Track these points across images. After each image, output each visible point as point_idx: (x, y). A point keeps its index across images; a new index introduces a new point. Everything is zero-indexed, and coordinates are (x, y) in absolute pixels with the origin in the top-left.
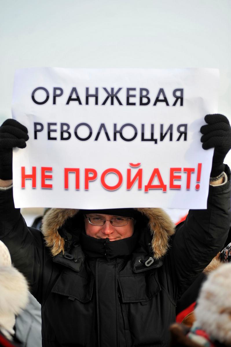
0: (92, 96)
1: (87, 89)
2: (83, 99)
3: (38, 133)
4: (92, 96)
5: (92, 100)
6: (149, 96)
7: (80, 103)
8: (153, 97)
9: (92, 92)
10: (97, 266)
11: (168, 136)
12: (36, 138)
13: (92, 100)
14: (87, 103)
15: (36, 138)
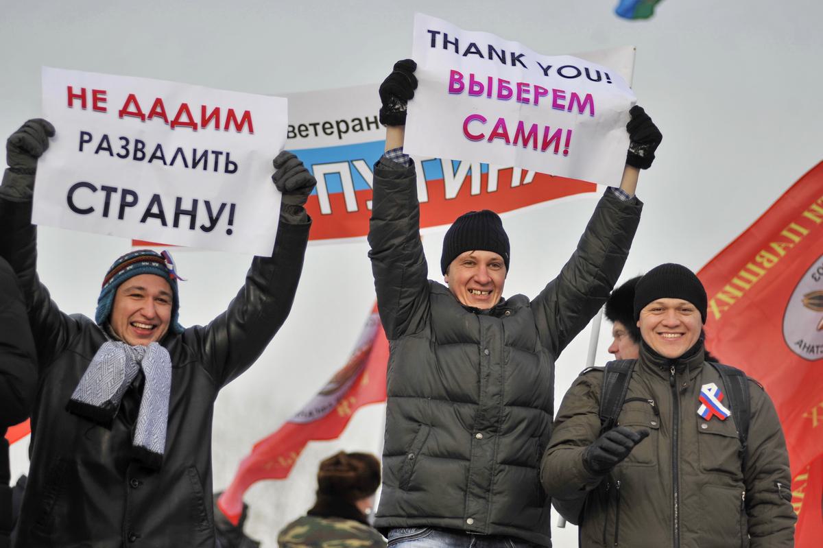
0: (186, 213)
1: (179, 200)
2: (170, 217)
3: (127, 209)
4: (186, 213)
5: (185, 220)
6: (145, 150)
7: (164, 223)
8: (149, 151)
9: (187, 205)
10: (206, 372)
11: (201, 164)
12: (121, 216)
13: (185, 220)
14: (176, 224)
15: (121, 216)
